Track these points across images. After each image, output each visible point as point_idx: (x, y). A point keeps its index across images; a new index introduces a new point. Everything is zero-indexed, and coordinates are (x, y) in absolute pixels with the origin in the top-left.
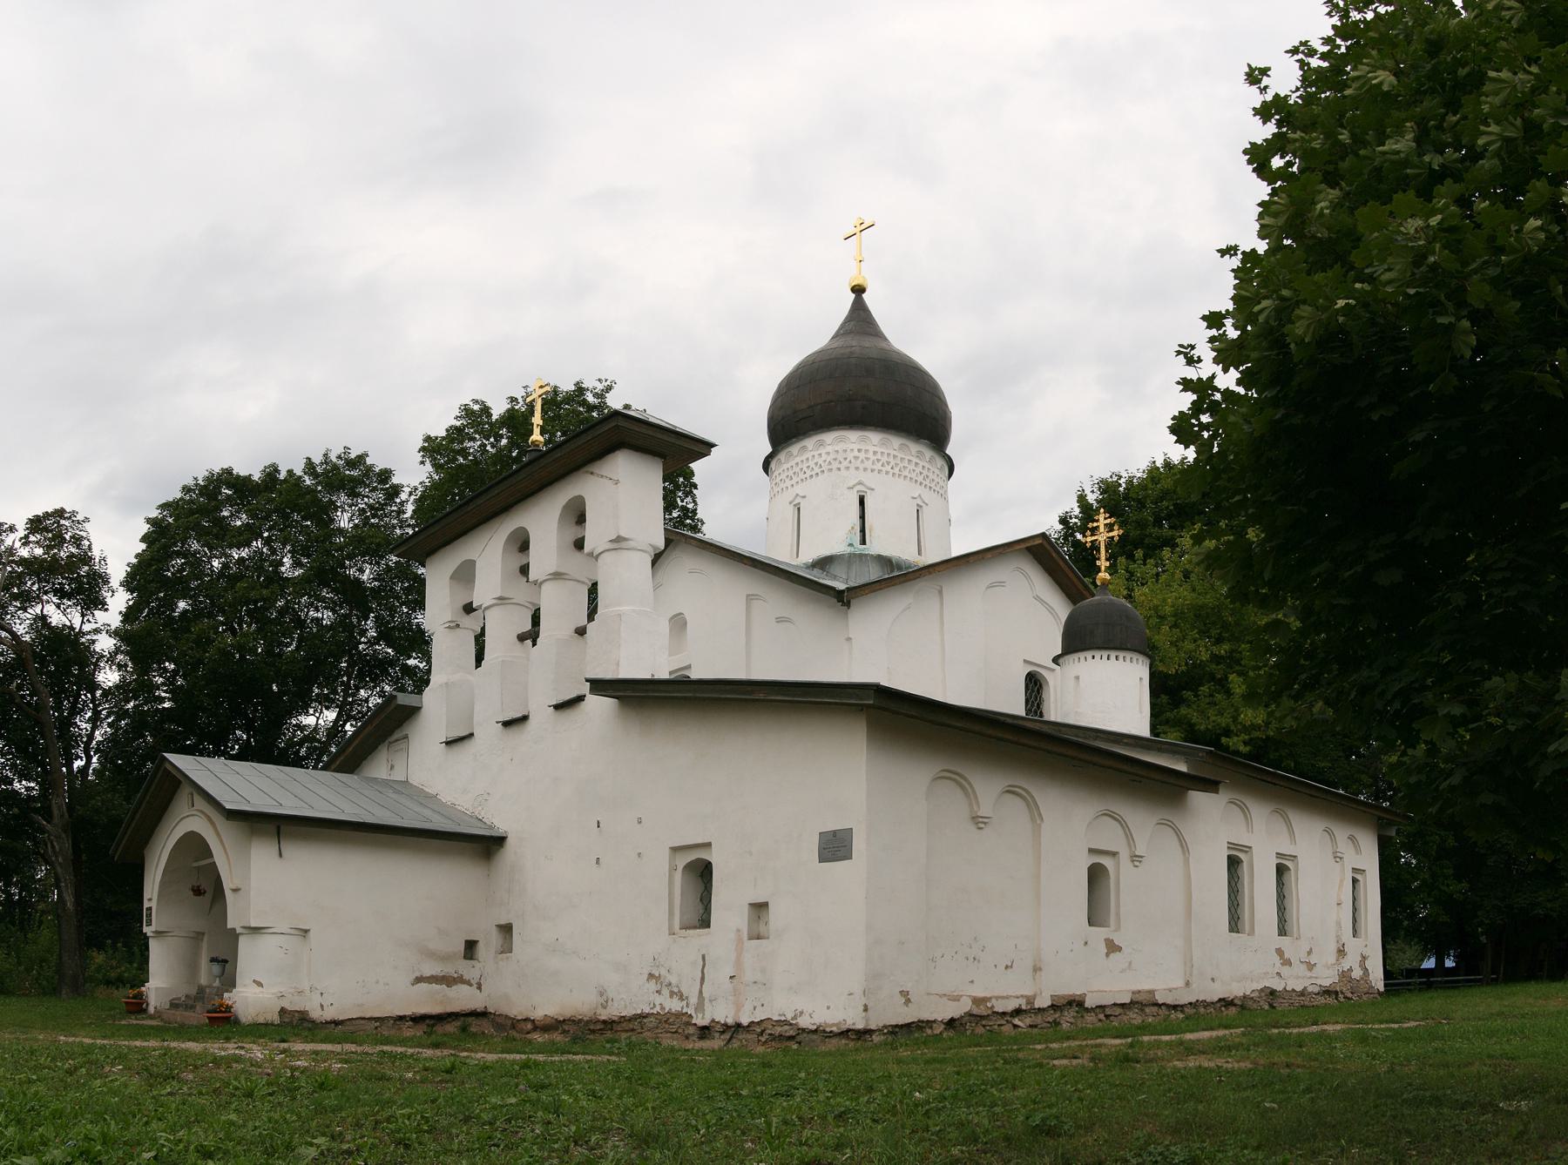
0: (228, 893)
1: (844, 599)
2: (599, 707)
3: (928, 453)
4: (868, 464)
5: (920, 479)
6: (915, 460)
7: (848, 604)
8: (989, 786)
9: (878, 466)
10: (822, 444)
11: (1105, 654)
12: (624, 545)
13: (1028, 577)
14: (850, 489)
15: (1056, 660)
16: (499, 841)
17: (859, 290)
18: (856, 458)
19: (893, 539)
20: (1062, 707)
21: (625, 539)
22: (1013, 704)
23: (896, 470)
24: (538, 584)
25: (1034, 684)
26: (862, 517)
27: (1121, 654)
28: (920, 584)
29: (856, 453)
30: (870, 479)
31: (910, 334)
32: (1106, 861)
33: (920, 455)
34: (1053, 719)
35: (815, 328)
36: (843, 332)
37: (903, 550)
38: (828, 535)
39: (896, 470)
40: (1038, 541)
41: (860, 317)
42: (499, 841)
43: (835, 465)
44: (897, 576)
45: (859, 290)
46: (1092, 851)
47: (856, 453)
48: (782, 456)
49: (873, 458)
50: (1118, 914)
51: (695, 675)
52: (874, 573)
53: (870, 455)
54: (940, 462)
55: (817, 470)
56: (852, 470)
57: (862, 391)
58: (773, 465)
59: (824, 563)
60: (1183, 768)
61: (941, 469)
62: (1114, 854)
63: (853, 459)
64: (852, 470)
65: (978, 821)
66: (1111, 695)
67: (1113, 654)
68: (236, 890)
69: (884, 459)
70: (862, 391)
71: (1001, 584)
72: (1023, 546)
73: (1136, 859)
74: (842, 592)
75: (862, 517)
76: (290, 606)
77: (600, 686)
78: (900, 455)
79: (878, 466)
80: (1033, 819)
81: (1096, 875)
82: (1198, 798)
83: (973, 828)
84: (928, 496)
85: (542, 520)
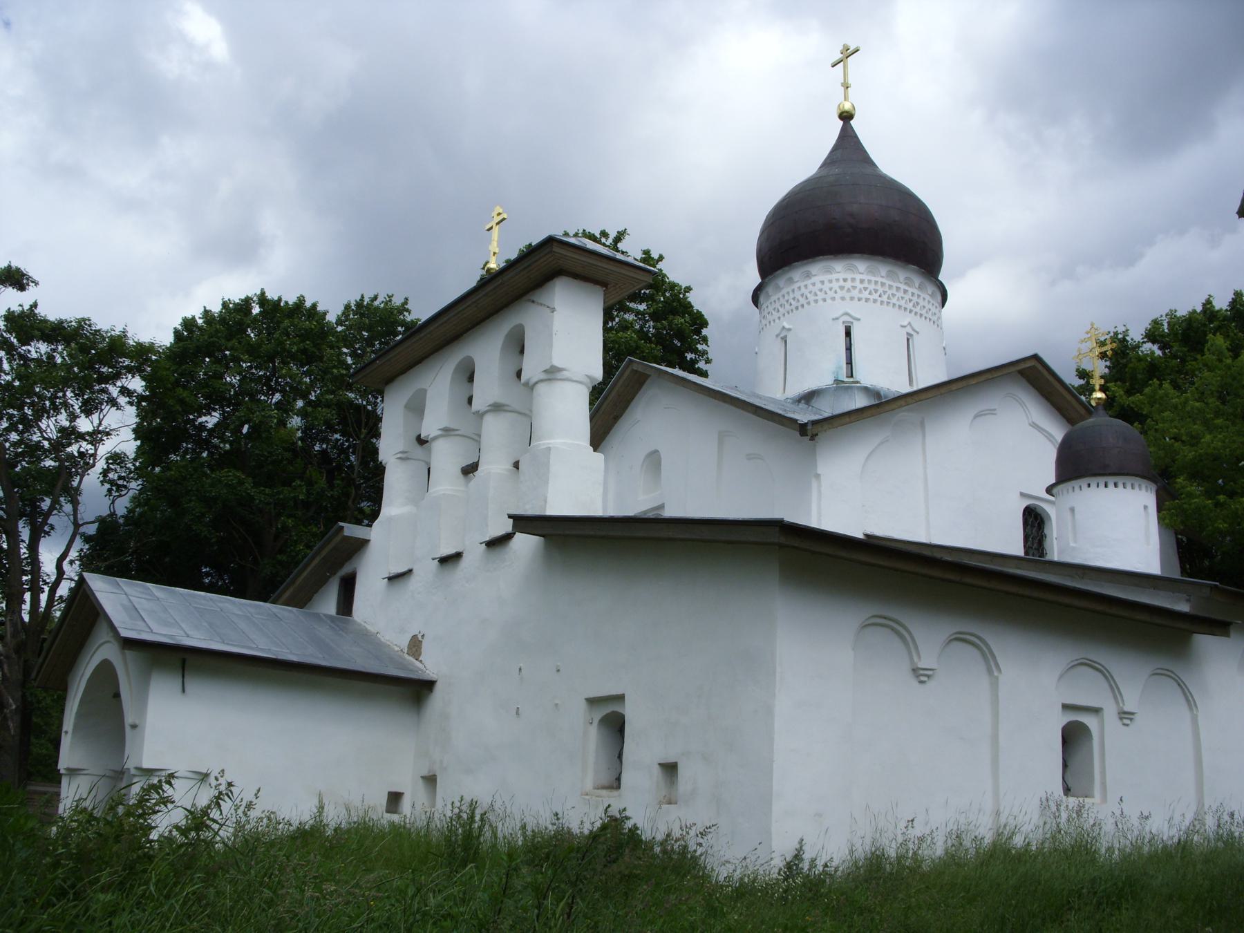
0: (128, 729)
1: (809, 432)
2: (525, 543)
3: (917, 280)
4: (855, 293)
5: (910, 306)
6: (903, 287)
7: (813, 437)
8: (931, 635)
9: (865, 294)
10: (808, 276)
11: (1102, 480)
12: (559, 375)
13: (1022, 404)
14: (852, 321)
15: (1049, 490)
16: (429, 685)
17: (846, 117)
18: (842, 288)
19: (883, 371)
20: (1064, 546)
21: (560, 370)
22: (1011, 542)
23: (885, 298)
24: (480, 415)
25: (1034, 520)
26: (849, 349)
27: (1120, 480)
28: (902, 414)
29: (841, 283)
30: (855, 309)
31: (895, 157)
32: (1089, 721)
33: (908, 282)
34: (1056, 558)
35: (802, 158)
36: (830, 162)
37: (897, 384)
38: (820, 369)
39: (885, 298)
40: (1028, 364)
41: (848, 143)
42: (429, 685)
43: (821, 296)
44: (883, 407)
45: (846, 117)
46: (1066, 707)
47: (841, 283)
48: (770, 289)
49: (881, 290)
50: (1104, 785)
51: (669, 513)
52: (860, 402)
53: (857, 284)
54: (931, 288)
55: (802, 301)
56: (838, 300)
57: (852, 219)
58: (762, 299)
59: (808, 398)
60: (1184, 607)
61: (932, 296)
62: (1096, 711)
63: (843, 291)
64: (838, 300)
65: (921, 675)
66: (1119, 530)
67: (1111, 480)
68: (134, 727)
69: (872, 287)
70: (852, 219)
71: (992, 412)
72: (1013, 369)
73: (1125, 716)
74: (806, 424)
75: (849, 349)
76: (264, 449)
77: (523, 523)
78: (888, 282)
79: (865, 294)
80: (990, 671)
81: (1073, 737)
82: (1205, 643)
83: (915, 683)
84: (919, 324)
85: (486, 352)
